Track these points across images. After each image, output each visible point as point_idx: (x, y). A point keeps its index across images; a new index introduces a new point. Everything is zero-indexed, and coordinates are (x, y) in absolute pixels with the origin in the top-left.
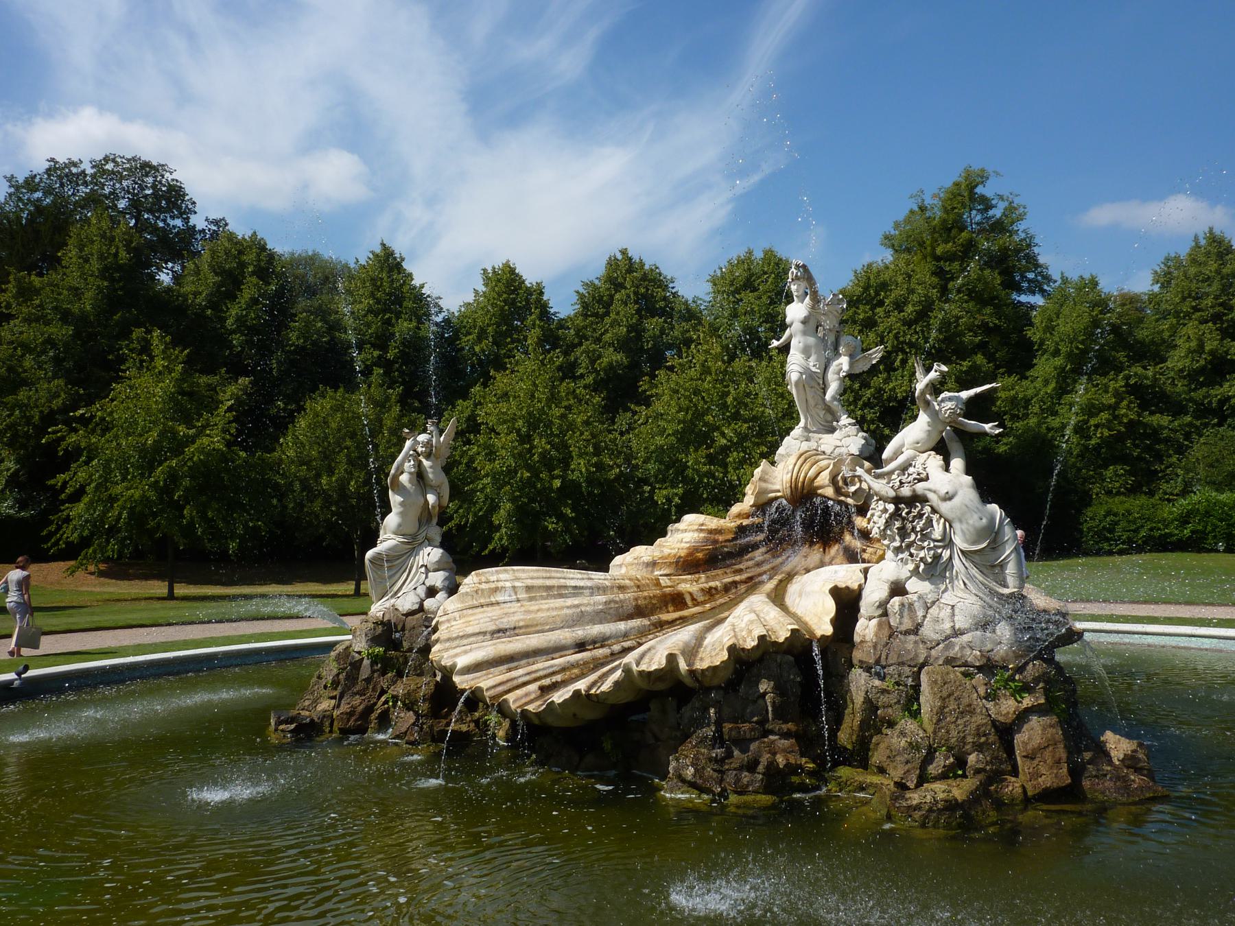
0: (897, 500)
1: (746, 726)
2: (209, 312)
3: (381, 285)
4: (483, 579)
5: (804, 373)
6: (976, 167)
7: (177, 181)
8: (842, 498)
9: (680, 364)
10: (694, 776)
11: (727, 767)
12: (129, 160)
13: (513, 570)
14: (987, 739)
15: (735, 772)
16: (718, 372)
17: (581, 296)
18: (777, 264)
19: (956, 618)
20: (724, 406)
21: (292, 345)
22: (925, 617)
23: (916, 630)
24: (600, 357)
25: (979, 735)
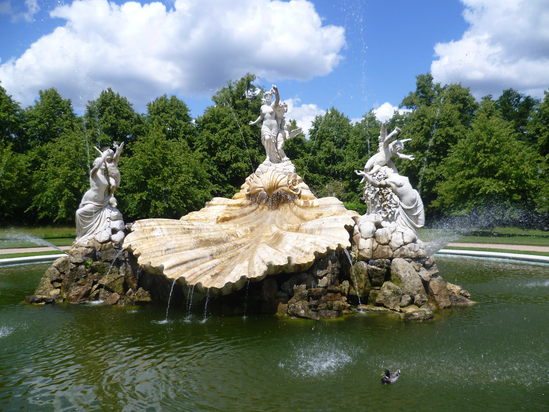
0: (380, 186)
4: (143, 225)
6: (252, 73)
10: (305, 314)
15: (324, 311)
19: (404, 237)
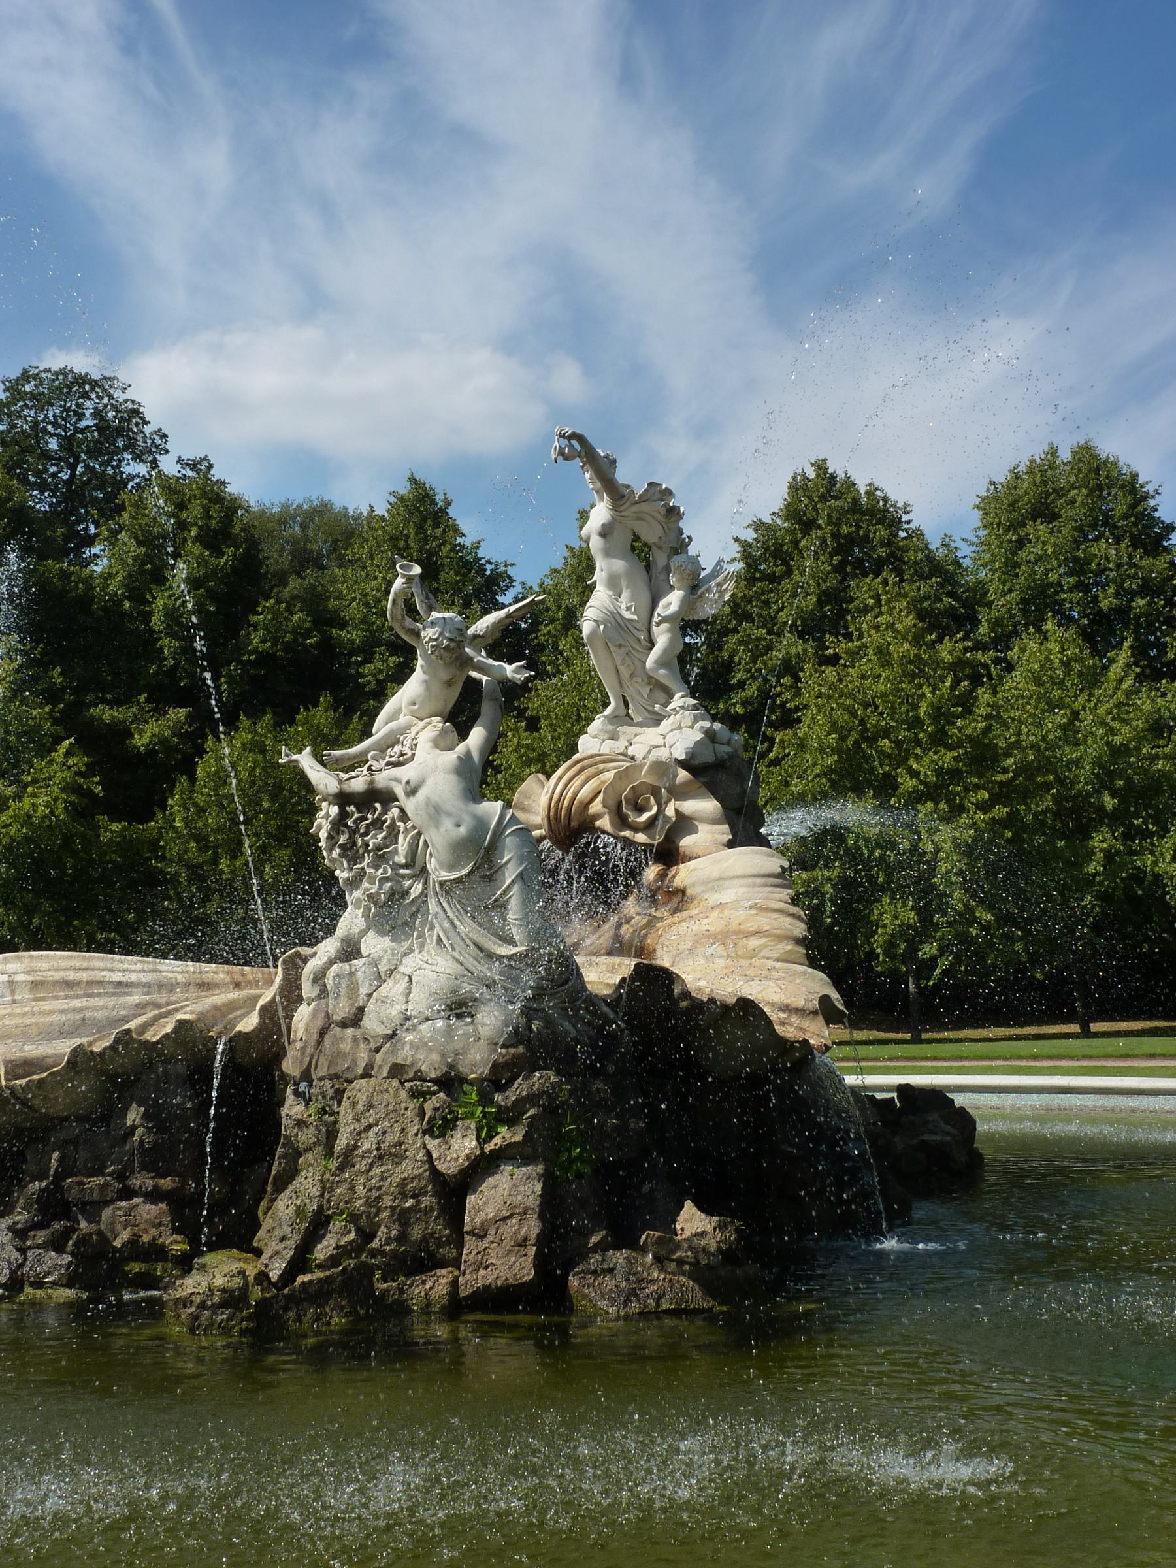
1: (96, 1181)
2: (127, 605)
3: (407, 547)
5: (605, 622)
7: (133, 402)
8: (627, 833)
9: (848, 652)
11: (29, 1243)
12: (56, 374)
13: (31, 957)
14: (418, 1203)
16: (906, 660)
17: (745, 545)
18: (1097, 471)
20: (915, 723)
21: (251, 653)
22: (370, 995)
23: (355, 1019)
24: (769, 648)
25: (405, 1196)
